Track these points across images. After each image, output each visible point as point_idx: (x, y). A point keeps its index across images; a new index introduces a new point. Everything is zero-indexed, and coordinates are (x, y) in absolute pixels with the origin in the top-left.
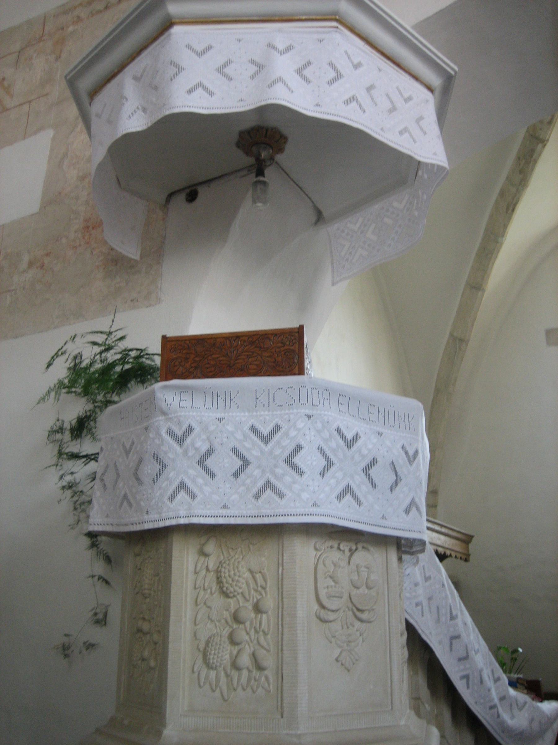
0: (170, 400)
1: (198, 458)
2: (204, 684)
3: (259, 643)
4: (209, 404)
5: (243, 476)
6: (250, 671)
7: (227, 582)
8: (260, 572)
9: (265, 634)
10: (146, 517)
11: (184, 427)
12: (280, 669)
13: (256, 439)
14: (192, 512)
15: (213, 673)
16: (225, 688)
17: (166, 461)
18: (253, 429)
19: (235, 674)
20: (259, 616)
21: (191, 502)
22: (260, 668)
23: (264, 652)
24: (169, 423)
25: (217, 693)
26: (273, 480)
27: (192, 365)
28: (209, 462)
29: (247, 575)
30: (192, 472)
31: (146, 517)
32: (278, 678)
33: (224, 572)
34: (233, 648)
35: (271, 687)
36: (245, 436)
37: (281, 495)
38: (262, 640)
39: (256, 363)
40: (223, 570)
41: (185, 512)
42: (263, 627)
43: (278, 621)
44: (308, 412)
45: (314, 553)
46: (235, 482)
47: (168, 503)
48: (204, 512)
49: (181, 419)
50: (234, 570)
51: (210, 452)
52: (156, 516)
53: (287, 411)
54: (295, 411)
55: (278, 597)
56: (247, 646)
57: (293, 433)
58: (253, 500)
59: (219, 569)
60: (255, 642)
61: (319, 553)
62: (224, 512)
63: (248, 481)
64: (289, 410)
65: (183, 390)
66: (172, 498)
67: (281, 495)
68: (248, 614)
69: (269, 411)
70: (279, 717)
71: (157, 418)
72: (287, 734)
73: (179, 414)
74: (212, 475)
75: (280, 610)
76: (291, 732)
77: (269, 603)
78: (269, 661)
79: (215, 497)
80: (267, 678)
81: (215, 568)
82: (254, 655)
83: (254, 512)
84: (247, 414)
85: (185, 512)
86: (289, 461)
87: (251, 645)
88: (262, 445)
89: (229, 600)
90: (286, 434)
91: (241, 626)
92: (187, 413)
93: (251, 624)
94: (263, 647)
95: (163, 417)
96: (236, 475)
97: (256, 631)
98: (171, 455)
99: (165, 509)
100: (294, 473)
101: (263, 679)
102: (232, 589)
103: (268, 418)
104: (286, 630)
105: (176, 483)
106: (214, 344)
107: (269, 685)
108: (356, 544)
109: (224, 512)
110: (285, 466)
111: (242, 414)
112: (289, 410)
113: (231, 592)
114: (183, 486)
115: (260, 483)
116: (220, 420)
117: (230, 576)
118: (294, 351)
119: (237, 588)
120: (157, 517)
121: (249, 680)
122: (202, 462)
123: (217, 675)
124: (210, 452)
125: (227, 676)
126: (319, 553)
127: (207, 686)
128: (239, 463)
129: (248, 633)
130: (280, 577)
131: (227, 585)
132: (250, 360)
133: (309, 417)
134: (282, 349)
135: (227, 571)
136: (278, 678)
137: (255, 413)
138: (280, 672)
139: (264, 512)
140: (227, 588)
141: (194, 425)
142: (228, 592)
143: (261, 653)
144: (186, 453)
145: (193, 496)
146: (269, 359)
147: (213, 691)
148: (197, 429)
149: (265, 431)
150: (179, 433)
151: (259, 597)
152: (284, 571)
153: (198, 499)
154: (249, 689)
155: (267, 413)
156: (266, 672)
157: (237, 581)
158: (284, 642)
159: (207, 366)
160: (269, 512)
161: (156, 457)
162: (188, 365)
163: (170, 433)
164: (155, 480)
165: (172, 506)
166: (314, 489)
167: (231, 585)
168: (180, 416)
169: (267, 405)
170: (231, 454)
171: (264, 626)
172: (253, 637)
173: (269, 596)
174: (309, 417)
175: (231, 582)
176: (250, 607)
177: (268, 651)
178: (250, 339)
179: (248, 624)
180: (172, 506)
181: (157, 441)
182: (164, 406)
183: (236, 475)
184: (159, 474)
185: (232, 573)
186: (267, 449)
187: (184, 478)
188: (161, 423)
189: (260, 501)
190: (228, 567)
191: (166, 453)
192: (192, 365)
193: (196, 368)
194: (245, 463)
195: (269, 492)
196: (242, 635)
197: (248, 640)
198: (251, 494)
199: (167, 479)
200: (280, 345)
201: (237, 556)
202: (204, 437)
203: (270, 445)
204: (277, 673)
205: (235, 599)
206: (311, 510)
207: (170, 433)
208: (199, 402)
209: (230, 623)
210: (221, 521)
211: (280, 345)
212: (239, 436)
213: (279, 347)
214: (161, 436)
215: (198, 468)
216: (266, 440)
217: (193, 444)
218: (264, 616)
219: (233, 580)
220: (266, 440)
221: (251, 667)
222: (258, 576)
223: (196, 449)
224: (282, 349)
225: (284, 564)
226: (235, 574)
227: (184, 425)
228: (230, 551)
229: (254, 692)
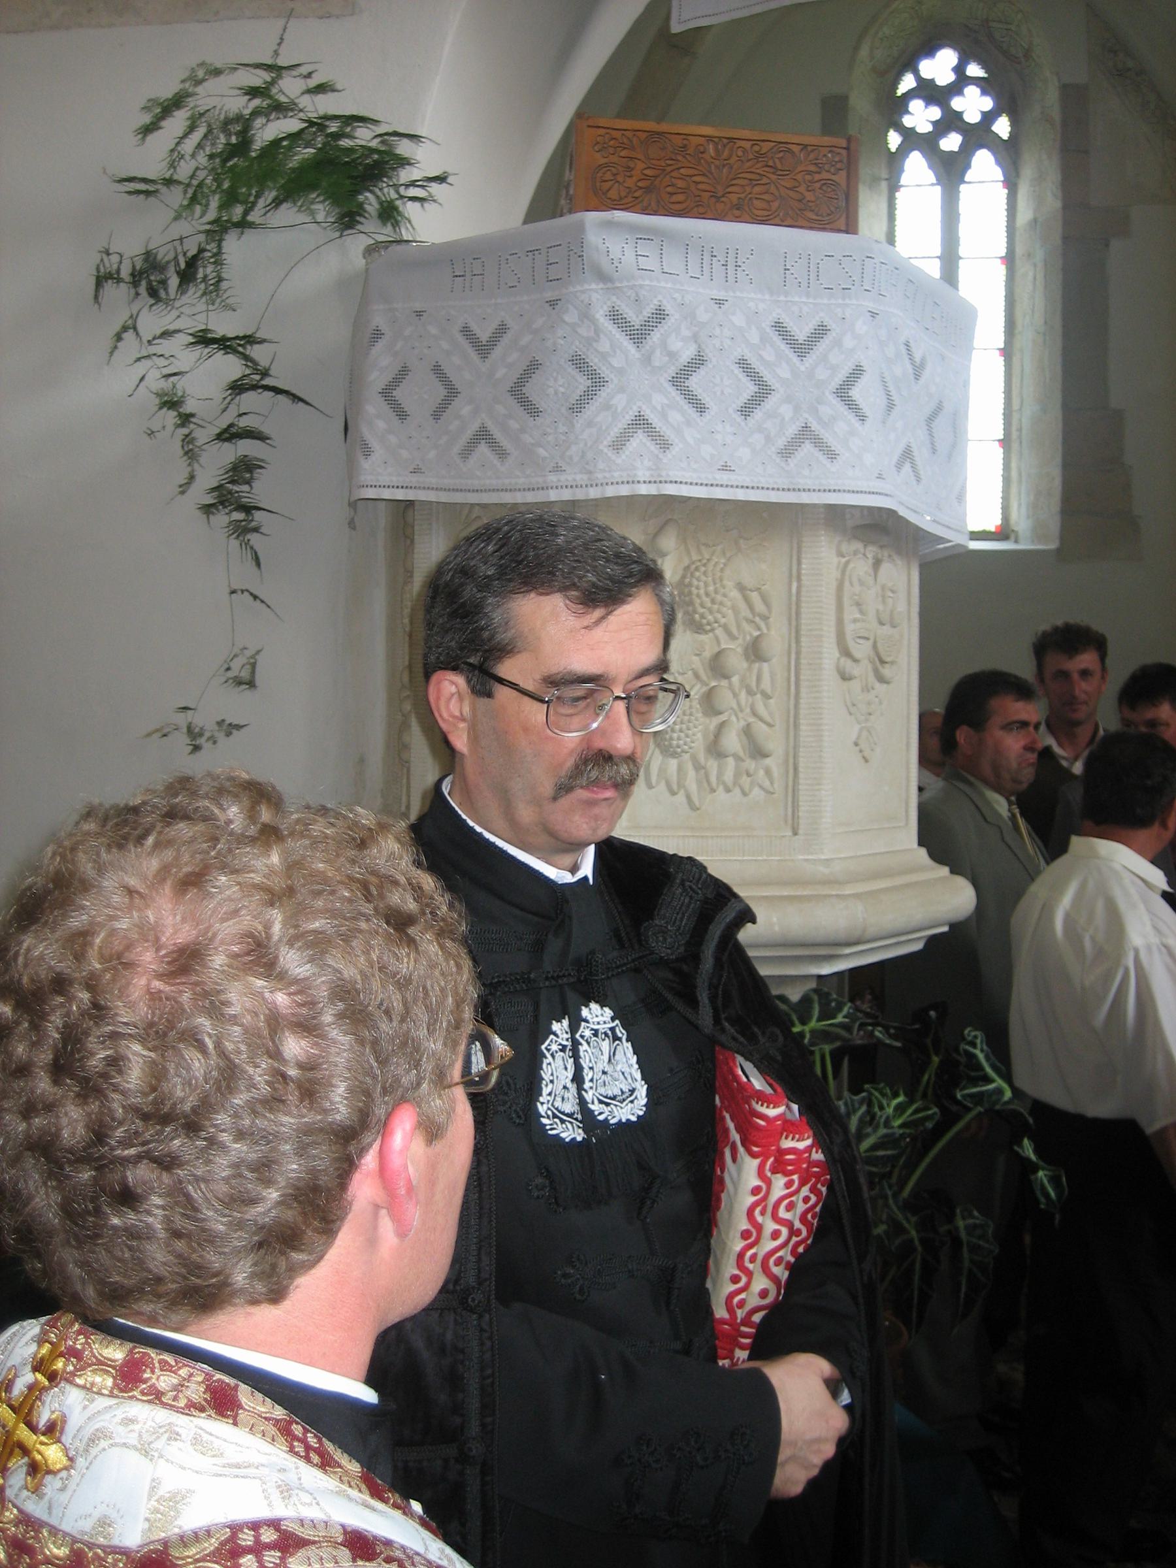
0: (615, 252)
1: (672, 371)
2: (658, 783)
3: (754, 714)
4: (694, 270)
5: (758, 414)
6: (738, 758)
7: (702, 605)
8: (758, 589)
9: (766, 696)
10: (552, 478)
11: (647, 312)
12: (791, 755)
13: (783, 346)
14: (664, 473)
15: (673, 763)
16: (693, 787)
17: (604, 371)
18: (779, 327)
19: (712, 765)
20: (757, 665)
21: (661, 456)
22: (758, 753)
23: (764, 726)
24: (614, 299)
25: (681, 797)
26: (815, 426)
27: (640, 184)
28: (695, 382)
29: (735, 594)
30: (658, 399)
31: (552, 478)
32: (787, 772)
33: (698, 588)
34: (708, 721)
35: (776, 786)
36: (764, 339)
37: (832, 455)
38: (761, 710)
39: (765, 197)
40: (695, 582)
41: (648, 473)
42: (763, 686)
43: (789, 675)
44: (871, 306)
45: (835, 560)
46: (743, 424)
47: (610, 453)
48: (688, 476)
49: (643, 292)
50: (715, 584)
51: (698, 362)
52: (578, 477)
53: (840, 301)
54: (854, 302)
55: (790, 634)
56: (734, 718)
57: (848, 342)
58: (778, 460)
59: (687, 580)
60: (748, 710)
61: (844, 560)
62: (724, 478)
63: (768, 425)
64: (844, 299)
65: (645, 235)
66: (619, 445)
67: (832, 455)
68: (736, 661)
69: (808, 295)
70: (789, 833)
71: (586, 286)
72: (806, 860)
73: (640, 282)
74: (701, 408)
75: (793, 656)
76: (810, 857)
77: (776, 639)
78: (774, 741)
79: (707, 450)
80: (768, 772)
81: (677, 578)
82: (747, 732)
83: (782, 482)
84: (767, 297)
85: (648, 473)
86: (843, 393)
87: (740, 715)
88: (795, 359)
89: (703, 637)
90: (838, 343)
91: (724, 683)
92: (655, 283)
93: (742, 680)
94: (762, 720)
95: (601, 286)
96: (746, 411)
97: (750, 693)
98: (616, 362)
99: (601, 465)
100: (851, 417)
101: (761, 773)
102: (710, 618)
103: (805, 309)
104: (803, 691)
105: (629, 417)
106: (685, 146)
107: (772, 783)
108: (865, 546)
109: (724, 478)
110: (835, 401)
111: (759, 296)
112: (844, 299)
113: (709, 624)
114: (640, 422)
115: (792, 430)
116: (720, 302)
117: (707, 595)
118: (836, 184)
119: (719, 616)
120: (581, 478)
121: (737, 775)
122: (679, 380)
123: (680, 769)
124: (698, 362)
125: (698, 767)
126: (844, 560)
127: (663, 785)
128: (750, 388)
129: (735, 695)
130: (794, 598)
131: (701, 610)
132: (757, 189)
133: (874, 315)
134: (817, 177)
135: (702, 584)
136: (787, 772)
137: (782, 298)
138: (791, 760)
139: (803, 482)
140: (702, 616)
141: (669, 308)
142: (704, 621)
143: (760, 728)
144: (647, 360)
145: (664, 445)
146: (791, 193)
147: (673, 793)
148: (674, 317)
149: (801, 333)
150: (636, 320)
151: (756, 633)
152: (804, 589)
153: (675, 450)
154: (737, 791)
155: (804, 299)
156: (768, 761)
157: (721, 603)
158: (802, 712)
159: (669, 189)
160: (809, 483)
161: (579, 363)
162: (630, 183)
163: (615, 317)
164: (577, 407)
165: (619, 461)
166: (718, 432)
167: (711, 611)
168: (641, 286)
169: (804, 284)
170: (738, 371)
171: (766, 684)
172: (743, 703)
173: (773, 632)
174: (874, 315)
175: (709, 605)
176: (739, 650)
177: (770, 725)
178: (756, 148)
179: (735, 680)
180: (621, 459)
181: (583, 331)
182: (605, 263)
183: (746, 411)
184: (588, 395)
185: (711, 588)
186: (804, 366)
187: (644, 407)
188: (595, 296)
189: (793, 462)
190: (703, 578)
191: (604, 356)
192: (640, 184)
193: (648, 190)
194: (763, 391)
195: (808, 447)
196: (725, 699)
197: (735, 706)
198: (773, 449)
199: (607, 407)
200: (813, 168)
201: (715, 559)
202: (686, 332)
203: (810, 360)
204: (786, 761)
205: (711, 634)
206: (718, 476)
207: (615, 317)
208: (673, 261)
209: (704, 678)
210: (720, 494)
211: (813, 168)
212: (754, 337)
213: (810, 173)
214: (593, 321)
215: (673, 392)
216: (801, 349)
217: (664, 344)
218: (765, 665)
219: (713, 602)
220: (801, 349)
221: (741, 754)
222: (755, 596)
223: (672, 355)
224: (817, 177)
225: (803, 578)
226: (716, 592)
227: (648, 304)
228: (703, 548)
229: (745, 794)
